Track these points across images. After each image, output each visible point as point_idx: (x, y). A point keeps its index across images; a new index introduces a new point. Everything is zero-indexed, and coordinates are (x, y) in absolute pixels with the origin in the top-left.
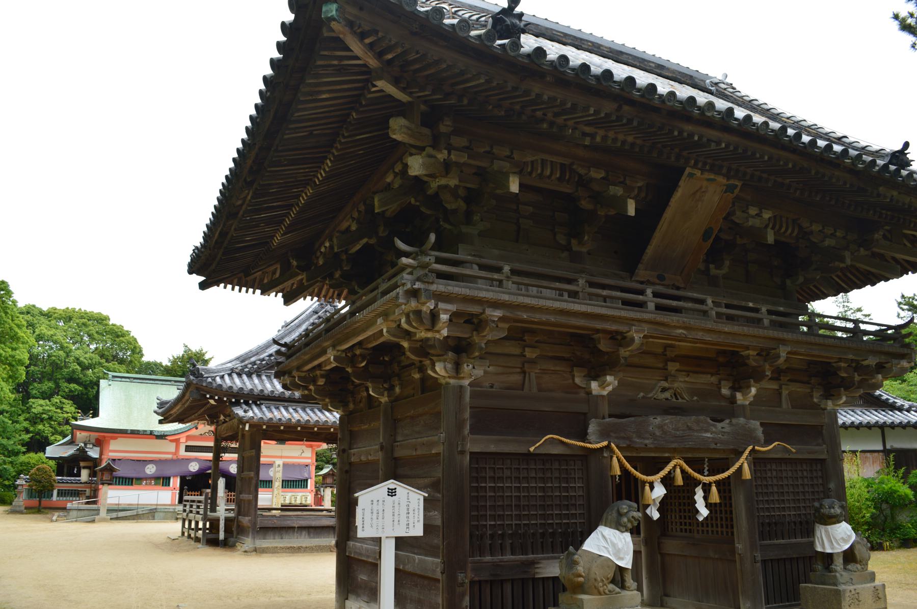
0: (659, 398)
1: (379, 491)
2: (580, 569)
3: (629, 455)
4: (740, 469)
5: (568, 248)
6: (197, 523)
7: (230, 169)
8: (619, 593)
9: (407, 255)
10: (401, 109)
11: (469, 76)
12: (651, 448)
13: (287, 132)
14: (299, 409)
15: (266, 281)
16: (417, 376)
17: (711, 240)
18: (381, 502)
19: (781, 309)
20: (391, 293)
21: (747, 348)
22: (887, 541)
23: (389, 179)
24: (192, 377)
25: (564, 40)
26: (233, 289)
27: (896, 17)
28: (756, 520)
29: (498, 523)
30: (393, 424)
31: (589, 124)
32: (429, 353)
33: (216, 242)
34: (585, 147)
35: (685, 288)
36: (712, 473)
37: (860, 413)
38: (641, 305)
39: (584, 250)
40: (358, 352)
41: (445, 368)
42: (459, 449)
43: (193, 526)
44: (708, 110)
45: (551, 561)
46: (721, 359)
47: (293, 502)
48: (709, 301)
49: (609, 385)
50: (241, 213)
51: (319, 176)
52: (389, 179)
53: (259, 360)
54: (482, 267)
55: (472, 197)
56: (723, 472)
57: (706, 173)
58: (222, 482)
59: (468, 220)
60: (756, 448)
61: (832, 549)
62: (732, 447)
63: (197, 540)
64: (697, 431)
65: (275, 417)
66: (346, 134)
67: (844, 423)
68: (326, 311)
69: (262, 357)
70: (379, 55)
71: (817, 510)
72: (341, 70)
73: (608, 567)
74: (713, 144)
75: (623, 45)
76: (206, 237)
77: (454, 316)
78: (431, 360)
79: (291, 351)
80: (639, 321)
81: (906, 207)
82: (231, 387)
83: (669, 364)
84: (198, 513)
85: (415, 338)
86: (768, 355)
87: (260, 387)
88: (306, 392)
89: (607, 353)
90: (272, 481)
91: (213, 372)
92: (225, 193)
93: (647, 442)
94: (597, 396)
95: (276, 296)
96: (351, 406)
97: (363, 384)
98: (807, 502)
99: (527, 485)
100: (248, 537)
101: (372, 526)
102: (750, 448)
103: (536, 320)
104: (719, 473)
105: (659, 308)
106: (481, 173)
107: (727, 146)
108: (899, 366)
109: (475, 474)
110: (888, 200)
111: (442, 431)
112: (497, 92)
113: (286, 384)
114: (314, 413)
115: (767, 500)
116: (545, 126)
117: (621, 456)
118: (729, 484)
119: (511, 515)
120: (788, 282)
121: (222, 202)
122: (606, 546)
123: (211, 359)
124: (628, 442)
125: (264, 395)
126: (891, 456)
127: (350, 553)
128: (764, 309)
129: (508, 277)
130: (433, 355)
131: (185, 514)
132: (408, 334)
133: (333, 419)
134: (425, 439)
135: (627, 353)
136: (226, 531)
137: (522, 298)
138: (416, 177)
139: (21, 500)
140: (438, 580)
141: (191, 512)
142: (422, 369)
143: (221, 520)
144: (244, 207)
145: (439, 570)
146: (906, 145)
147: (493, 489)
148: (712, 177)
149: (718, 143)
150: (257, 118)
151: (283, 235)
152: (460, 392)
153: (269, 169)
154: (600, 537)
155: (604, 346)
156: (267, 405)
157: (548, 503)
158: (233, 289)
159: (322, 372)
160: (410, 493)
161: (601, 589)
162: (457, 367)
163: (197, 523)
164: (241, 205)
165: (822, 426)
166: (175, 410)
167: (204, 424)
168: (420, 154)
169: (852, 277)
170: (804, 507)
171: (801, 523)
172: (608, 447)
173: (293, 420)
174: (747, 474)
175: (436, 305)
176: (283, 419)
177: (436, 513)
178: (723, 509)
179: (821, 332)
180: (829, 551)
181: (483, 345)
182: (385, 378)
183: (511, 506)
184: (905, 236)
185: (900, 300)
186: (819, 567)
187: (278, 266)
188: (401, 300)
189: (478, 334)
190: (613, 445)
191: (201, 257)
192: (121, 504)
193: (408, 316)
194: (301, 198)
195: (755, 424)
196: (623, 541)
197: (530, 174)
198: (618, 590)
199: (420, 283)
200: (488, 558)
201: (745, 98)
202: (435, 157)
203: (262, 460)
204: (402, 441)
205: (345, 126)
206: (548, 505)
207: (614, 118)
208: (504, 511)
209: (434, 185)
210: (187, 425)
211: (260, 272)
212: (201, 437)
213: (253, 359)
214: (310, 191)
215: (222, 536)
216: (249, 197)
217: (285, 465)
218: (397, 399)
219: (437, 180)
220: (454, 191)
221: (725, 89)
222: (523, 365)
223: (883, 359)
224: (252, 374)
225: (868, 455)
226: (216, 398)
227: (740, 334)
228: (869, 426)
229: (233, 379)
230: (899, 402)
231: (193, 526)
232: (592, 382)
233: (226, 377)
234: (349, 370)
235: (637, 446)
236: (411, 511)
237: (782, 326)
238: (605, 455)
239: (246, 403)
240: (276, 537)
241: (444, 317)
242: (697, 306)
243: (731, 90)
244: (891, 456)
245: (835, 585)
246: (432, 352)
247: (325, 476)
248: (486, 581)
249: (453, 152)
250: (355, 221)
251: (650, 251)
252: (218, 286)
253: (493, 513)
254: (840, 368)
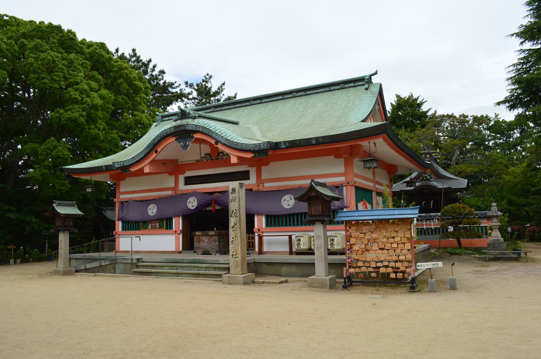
139: (304, 225)
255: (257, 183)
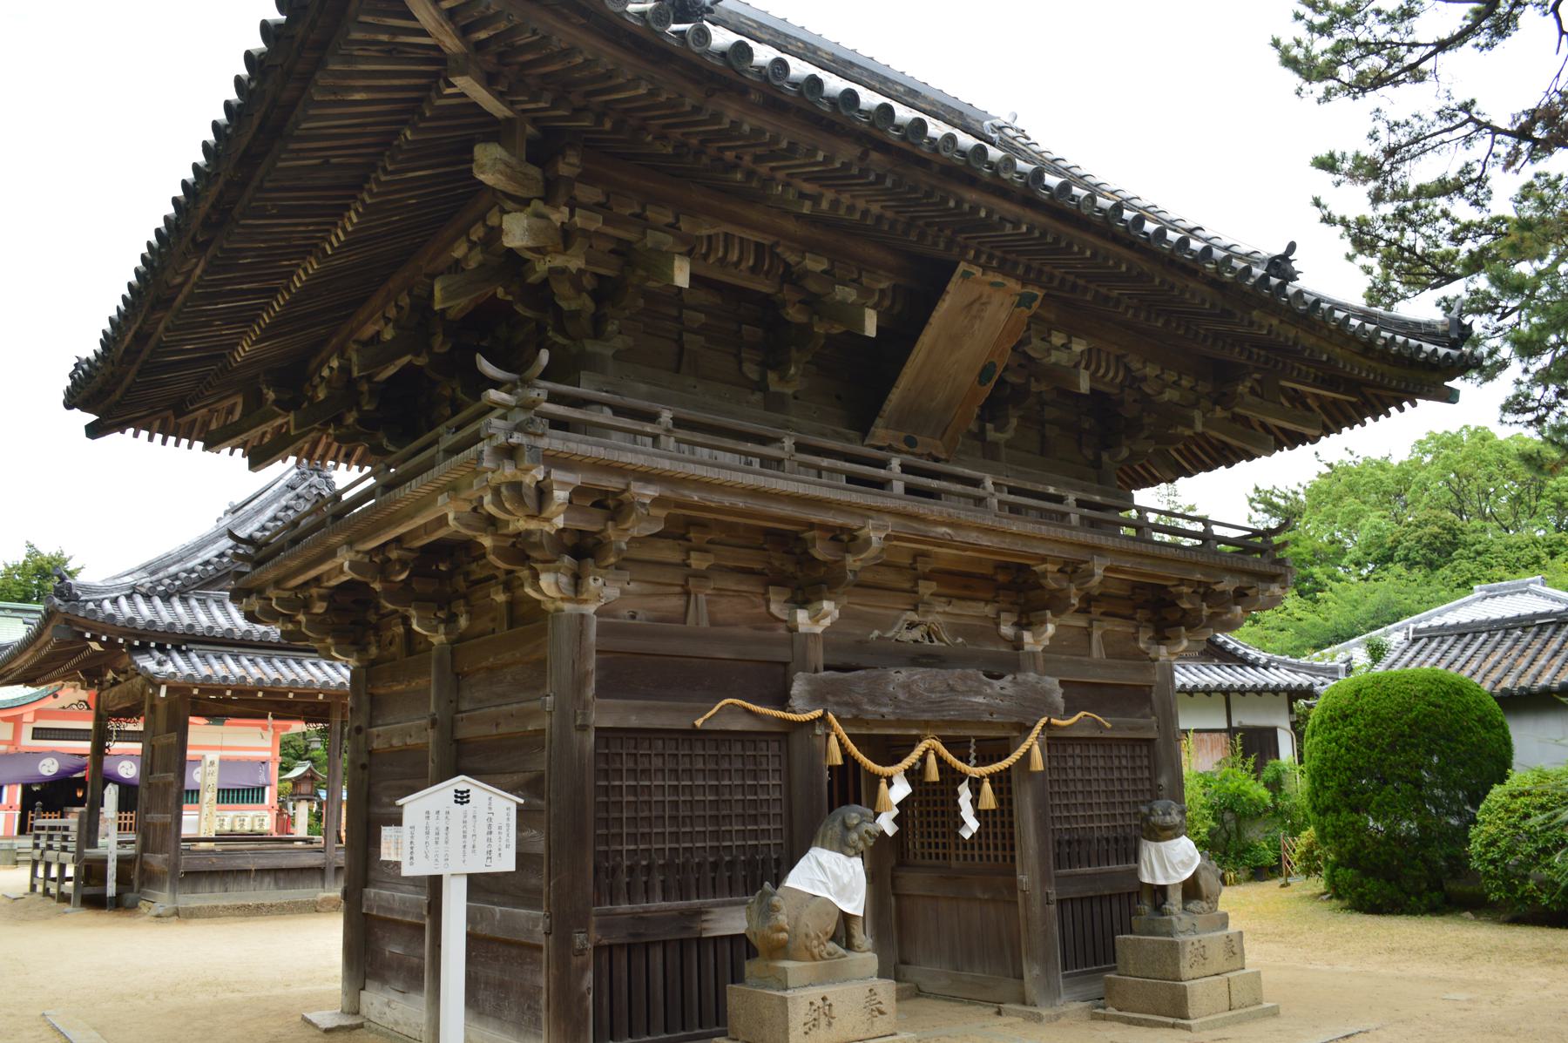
0: (904, 639)
1: (439, 796)
2: (782, 919)
3: (855, 731)
4: (1027, 755)
5: (761, 386)
6: (62, 868)
7: (166, 218)
8: (844, 956)
9: (497, 384)
10: (494, 130)
11: (621, 80)
12: (889, 721)
13: (283, 156)
14: (259, 660)
15: (213, 426)
16: (501, 598)
17: (993, 383)
18: (443, 815)
19: (1098, 498)
20: (467, 452)
21: (1044, 559)
22: (1230, 870)
23: (459, 251)
24: (57, 601)
25: (758, 34)
26: (151, 439)
27: (1276, 44)
28: (1050, 836)
29: (642, 847)
30: (456, 678)
31: (810, 178)
32: (528, 557)
33: (127, 350)
34: (799, 217)
35: (947, 461)
36: (983, 760)
37: (1195, 671)
38: (882, 485)
39: (789, 391)
40: (394, 555)
41: (557, 583)
42: (578, 723)
43: (54, 872)
44: (1005, 168)
45: (729, 909)
46: (1001, 578)
47: (237, 828)
48: (989, 482)
49: (825, 616)
50: (181, 298)
51: (333, 239)
52: (459, 251)
53: (185, 571)
54: (618, 411)
55: (605, 292)
56: (1000, 759)
57: (991, 273)
58: (113, 792)
59: (598, 333)
60: (1053, 721)
61: (1166, 878)
62: (1015, 719)
63: (63, 898)
64: (963, 693)
65: (215, 673)
66: (390, 168)
67: (1184, 685)
68: (310, 486)
69: (189, 565)
70: (464, 32)
71: (1146, 818)
72: (392, 52)
73: (828, 914)
74: (1009, 226)
75: (855, 51)
76: (108, 341)
77: (578, 492)
78: (532, 569)
79: (261, 554)
80: (879, 510)
81: (1290, 343)
82: (132, 620)
83: (921, 583)
84: (64, 849)
85: (505, 531)
86: (1074, 572)
87: (187, 621)
88: (290, 626)
89: (825, 563)
90: (198, 791)
91: (97, 590)
92: (153, 261)
93: (884, 710)
94: (806, 635)
95: (231, 453)
96: (373, 651)
97: (397, 611)
98: (1127, 806)
99: (690, 783)
100: (161, 890)
101: (427, 857)
102: (1044, 720)
103: (713, 505)
104: (992, 761)
105: (910, 490)
106: (623, 251)
107: (1030, 229)
108: (1267, 594)
109: (603, 766)
110: (1265, 332)
111: (548, 690)
112: (663, 112)
113: (253, 612)
114: (288, 666)
115: (1067, 805)
116: (739, 176)
117: (843, 733)
118: (1009, 780)
119: (664, 833)
120: (1105, 457)
121: (145, 279)
122: (823, 879)
123: (79, 570)
124: (854, 711)
125: (194, 635)
126: (1238, 737)
127: (370, 908)
128: (1071, 498)
129: (668, 430)
130: (537, 561)
131: (38, 852)
132: (491, 523)
133: (340, 680)
134: (515, 706)
135: (858, 563)
136: (118, 881)
137: (692, 466)
138: (510, 250)
140: (539, 948)
141: (50, 847)
142: (510, 584)
143: (110, 860)
144: (186, 290)
145: (541, 928)
146: (1292, 247)
147: (633, 790)
148: (999, 279)
149: (1016, 224)
150: (226, 126)
151: (254, 343)
152: (581, 624)
153: (242, 222)
154: (814, 864)
155: (821, 551)
156: (200, 652)
157: (724, 812)
158: (151, 439)
159: (322, 591)
160: (494, 797)
161: (816, 951)
162: (577, 580)
163: (62, 868)
164: (182, 285)
165: (1150, 687)
166: (20, 662)
167: (74, 687)
168: (521, 211)
169: (1199, 453)
170: (1122, 815)
171: (1116, 840)
172: (822, 719)
173: (250, 680)
174: (1038, 763)
175: (548, 474)
176: (232, 678)
177: (535, 832)
178: (998, 819)
179: (1157, 537)
180: (1161, 882)
181: (624, 546)
182: (442, 603)
183: (663, 817)
184: (1283, 390)
185: (1252, 495)
186: (1146, 907)
187: (239, 400)
188: (487, 464)
189: (616, 526)
190: (831, 716)
191: (94, 377)
193: (496, 491)
194: (295, 278)
195: (1052, 683)
196: (851, 871)
197: (705, 257)
198: (842, 951)
199: (520, 435)
200: (624, 907)
201: (1045, 155)
202: (549, 219)
203: (190, 753)
204: (474, 710)
205: (388, 153)
206: (724, 817)
207: (855, 171)
208: (650, 826)
209: (542, 266)
210: (42, 688)
211: (204, 411)
212: (64, 712)
213: (173, 569)
214: (313, 266)
215: (111, 889)
216: (198, 271)
217: (224, 763)
218: (462, 638)
219: (548, 259)
220: (576, 279)
221: (1014, 138)
222: (687, 582)
223: (1244, 581)
224: (171, 595)
225: (1205, 736)
226: (104, 638)
227: (1034, 538)
228: (1208, 691)
229: (135, 604)
230: (1253, 654)
231: (54, 872)
232: (799, 611)
233: (123, 601)
234: (377, 586)
235: (869, 717)
236: (495, 830)
237: (1093, 524)
238: (818, 732)
239: (161, 648)
240: (216, 889)
241: (560, 495)
242: (970, 490)
243: (1024, 141)
244: (1238, 737)
245: (1170, 934)
246: (534, 554)
247: (296, 782)
248: (621, 946)
249: (578, 211)
250: (391, 325)
251: (895, 396)
252: (123, 432)
253: (633, 830)
254: (1180, 596)
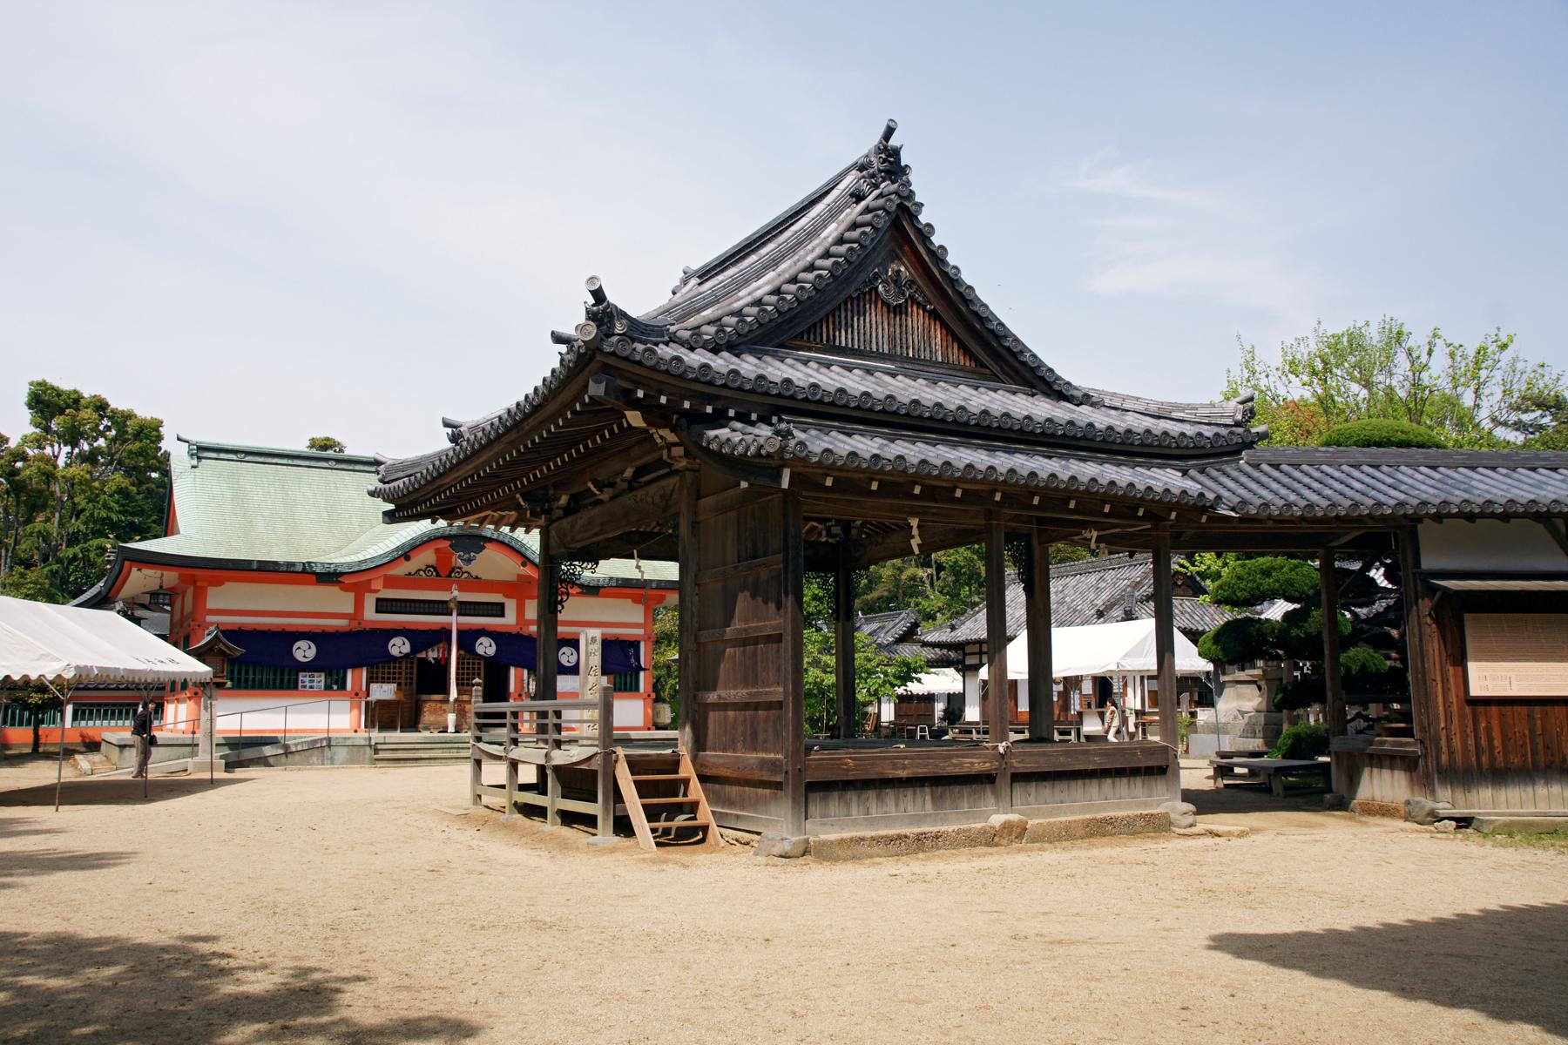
192: (290, 731)
255: (517, 624)
